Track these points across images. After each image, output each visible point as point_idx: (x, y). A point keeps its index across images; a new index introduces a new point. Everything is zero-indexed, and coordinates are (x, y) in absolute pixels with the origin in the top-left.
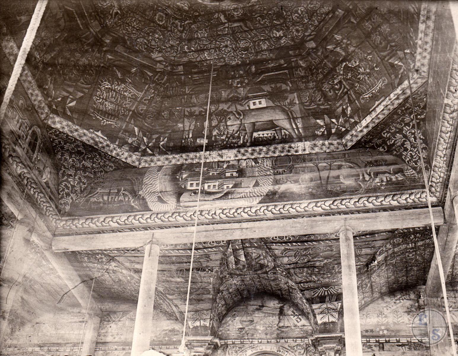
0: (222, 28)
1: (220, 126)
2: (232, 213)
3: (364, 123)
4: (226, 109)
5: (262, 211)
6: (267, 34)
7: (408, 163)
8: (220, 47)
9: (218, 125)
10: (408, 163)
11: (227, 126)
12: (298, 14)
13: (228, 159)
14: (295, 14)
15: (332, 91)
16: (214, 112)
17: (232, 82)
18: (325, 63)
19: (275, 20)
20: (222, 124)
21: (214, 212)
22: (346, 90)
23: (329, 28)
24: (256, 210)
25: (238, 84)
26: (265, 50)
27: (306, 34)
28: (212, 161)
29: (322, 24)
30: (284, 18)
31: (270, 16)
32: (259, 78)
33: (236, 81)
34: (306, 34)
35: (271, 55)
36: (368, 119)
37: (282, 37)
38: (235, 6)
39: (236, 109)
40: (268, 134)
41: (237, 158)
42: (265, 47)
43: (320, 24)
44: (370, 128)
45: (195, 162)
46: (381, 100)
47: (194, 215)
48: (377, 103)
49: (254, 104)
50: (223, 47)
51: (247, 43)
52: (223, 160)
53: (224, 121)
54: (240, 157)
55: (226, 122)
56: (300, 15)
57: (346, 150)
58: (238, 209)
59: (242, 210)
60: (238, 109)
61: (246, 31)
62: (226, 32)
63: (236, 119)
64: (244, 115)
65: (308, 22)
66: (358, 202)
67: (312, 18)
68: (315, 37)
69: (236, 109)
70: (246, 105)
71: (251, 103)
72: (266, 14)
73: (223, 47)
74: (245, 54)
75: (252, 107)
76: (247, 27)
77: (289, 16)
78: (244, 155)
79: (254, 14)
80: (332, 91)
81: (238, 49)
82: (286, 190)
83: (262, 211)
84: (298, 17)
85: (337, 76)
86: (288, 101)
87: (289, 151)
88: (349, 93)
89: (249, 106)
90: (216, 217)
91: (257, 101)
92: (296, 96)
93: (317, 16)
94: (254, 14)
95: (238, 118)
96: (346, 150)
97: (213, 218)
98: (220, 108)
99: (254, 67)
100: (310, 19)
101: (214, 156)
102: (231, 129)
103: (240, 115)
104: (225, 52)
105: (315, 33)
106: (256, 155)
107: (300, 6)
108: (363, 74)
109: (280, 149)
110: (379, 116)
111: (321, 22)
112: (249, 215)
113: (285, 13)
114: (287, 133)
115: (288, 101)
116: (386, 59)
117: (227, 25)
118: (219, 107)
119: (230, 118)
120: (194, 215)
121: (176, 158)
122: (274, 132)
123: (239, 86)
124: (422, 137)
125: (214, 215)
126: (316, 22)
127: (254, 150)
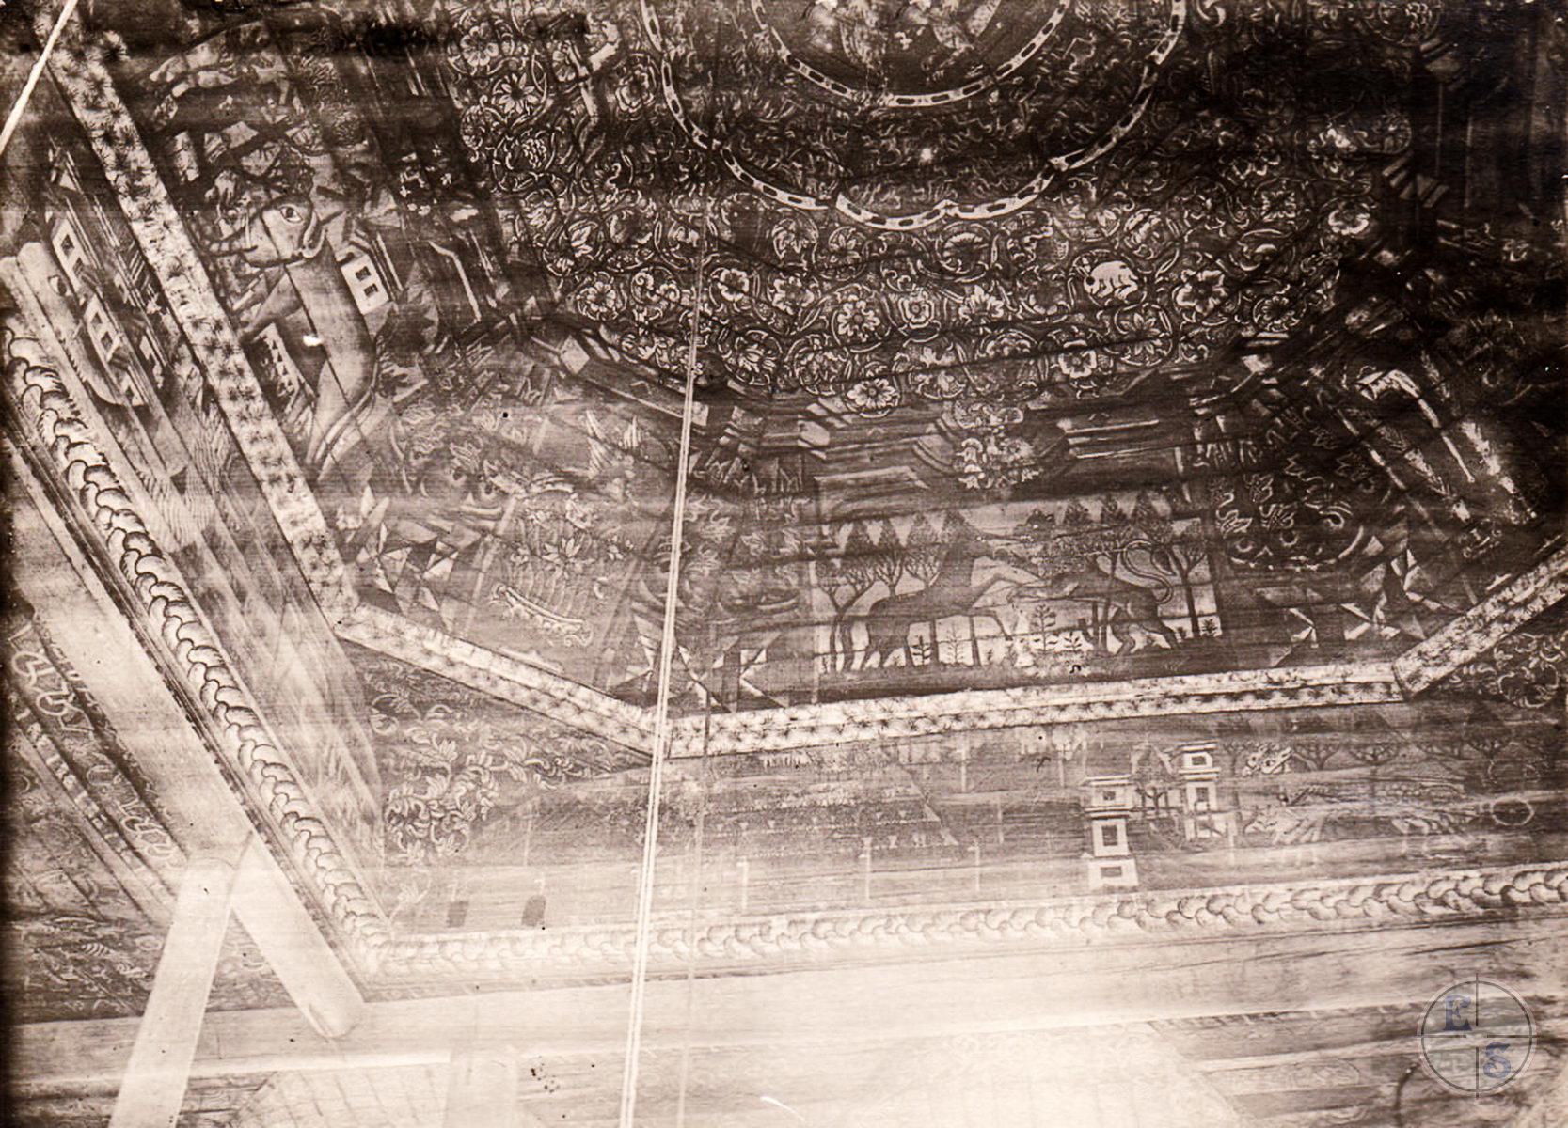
0: (573, 58)
1: (249, 188)
2: (103, 500)
3: (460, 651)
4: (317, 182)
5: (157, 591)
6: (576, 210)
7: (390, 818)
8: (510, 72)
9: (252, 178)
10: (390, 818)
11: (259, 214)
12: (656, 286)
13: (174, 300)
14: (652, 273)
15: (464, 478)
16: (291, 141)
17: (410, 163)
18: (539, 424)
19: (620, 220)
20: (261, 193)
21: (75, 438)
22: (490, 524)
23: (645, 397)
24: (151, 575)
25: (407, 185)
26: (1399, 1092)
27: (603, 331)
28: (144, 242)
29: (652, 372)
30: (629, 241)
31: (629, 199)
32: (443, 246)
33: (416, 176)
34: (603, 331)
35: (515, 248)
36: (481, 659)
37: (573, 258)
38: (646, 83)
39: (328, 220)
40: (285, 373)
41: (188, 328)
42: (536, 219)
43: (647, 363)
44: (449, 673)
45: (111, 176)
46: (547, 665)
47: (30, 369)
48: (532, 658)
49: (362, 274)
50: (512, 84)
51: (541, 158)
52: (165, 284)
53: (275, 194)
54: (198, 337)
55: (272, 205)
56: (653, 293)
57: (332, 629)
58: (129, 513)
59: (133, 528)
60: (330, 226)
61: (575, 142)
62: (561, 79)
63: (296, 236)
64: (317, 258)
65: (641, 324)
66: (299, 819)
67: (658, 335)
68: (606, 363)
69: (328, 220)
70: (352, 249)
71: (364, 261)
72: (632, 186)
73: (512, 84)
74: (503, 166)
75: (349, 271)
76: (587, 144)
77: (641, 257)
78: (211, 347)
79: (631, 149)
80: (464, 478)
81: (517, 137)
82: (17, 478)
83: (157, 591)
84: (644, 287)
85: (519, 482)
86: (398, 371)
87: (275, 480)
88: (488, 539)
89: (350, 258)
90: (60, 455)
91: (374, 279)
92: (417, 387)
93: (669, 350)
94: (631, 149)
95: (300, 244)
96: (332, 629)
97: (54, 448)
98: (314, 161)
99: (474, 212)
100: (649, 328)
101: (169, 244)
102: (253, 238)
103: (312, 247)
104: (498, 96)
105: (617, 358)
106: (222, 386)
107: (679, 285)
108: (563, 556)
109: (274, 453)
110: (503, 684)
111: (654, 366)
112: (122, 561)
113: (643, 241)
114: (308, 428)
115: (398, 371)
116: (635, 605)
117: (583, 71)
118: (317, 154)
119: (289, 214)
120: (30, 369)
121: (101, 94)
122: (297, 387)
123: (404, 192)
124: (483, 811)
125: (63, 445)
126: (651, 351)
127: (241, 372)
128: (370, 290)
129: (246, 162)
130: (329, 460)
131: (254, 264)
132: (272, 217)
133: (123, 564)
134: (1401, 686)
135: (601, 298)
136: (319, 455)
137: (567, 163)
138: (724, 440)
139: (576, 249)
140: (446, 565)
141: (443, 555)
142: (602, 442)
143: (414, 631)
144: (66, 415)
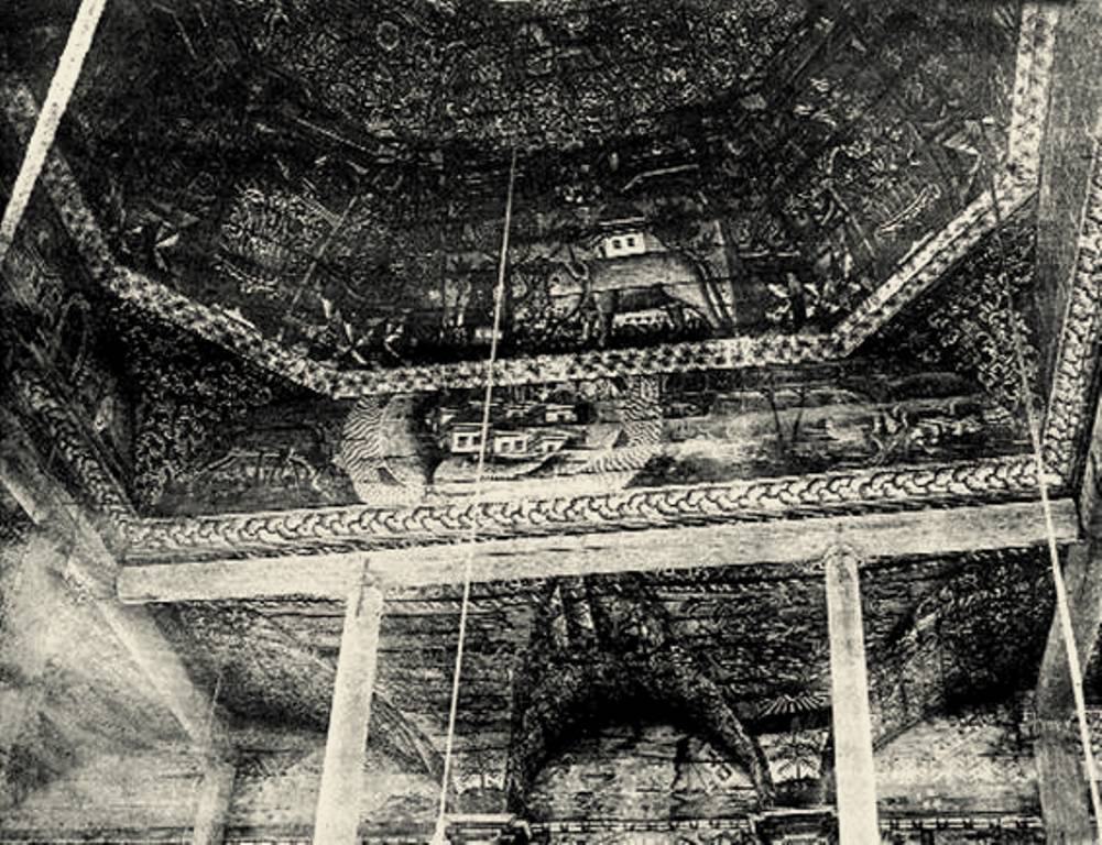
3: (884, 294)
11: (549, 297)
36: (895, 283)
39: (573, 256)
49: (617, 245)
55: (547, 289)
69: (573, 256)
75: (611, 252)
78: (590, 368)
89: (603, 250)
91: (623, 240)
123: (580, 200)
128: (631, 243)
129: (516, 295)
130: (729, 310)
131: (573, 314)
132: (554, 291)
133: (605, 517)
134: (120, 233)
135: (722, 69)
136: (720, 315)
137: (607, 77)
138: (852, 13)
139: (679, 79)
140: (848, 259)
141: (843, 256)
142: (817, 109)
143: (858, 313)
144: (500, 508)
